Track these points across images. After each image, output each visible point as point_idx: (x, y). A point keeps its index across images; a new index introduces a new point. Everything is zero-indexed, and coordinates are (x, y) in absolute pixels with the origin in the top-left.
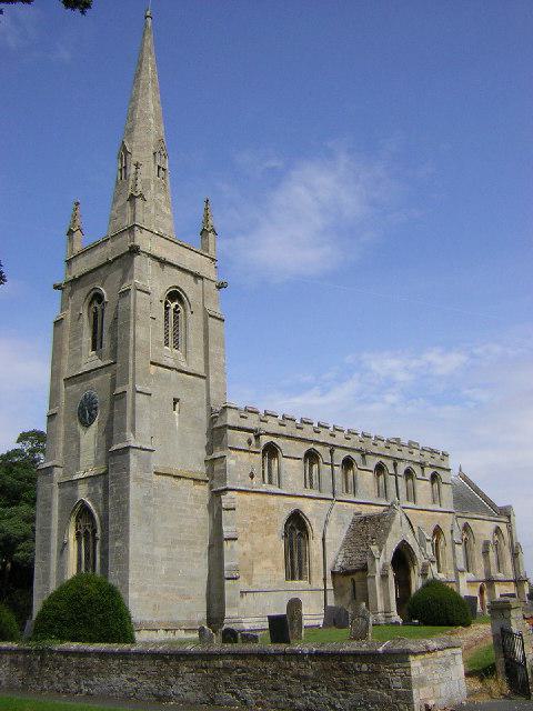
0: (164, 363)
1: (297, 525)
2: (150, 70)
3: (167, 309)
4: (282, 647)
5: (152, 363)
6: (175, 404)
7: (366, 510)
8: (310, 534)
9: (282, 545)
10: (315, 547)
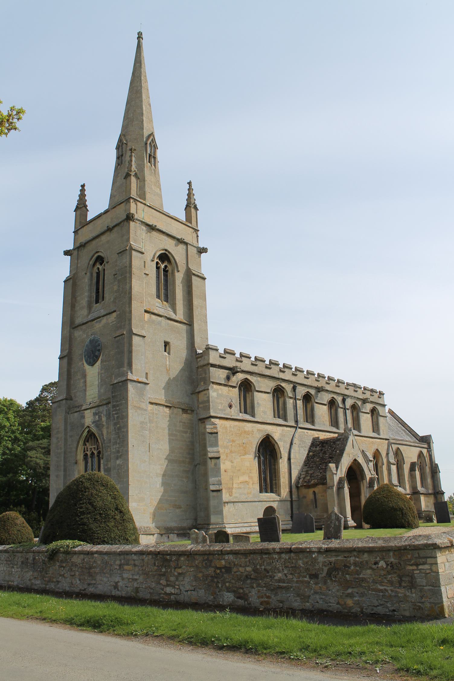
0: (156, 312)
1: (267, 450)
2: (362, 507)
3: (158, 268)
4: (273, 545)
5: (146, 311)
6: (165, 346)
7: (323, 436)
8: (279, 456)
9: (255, 464)
10: (283, 465)
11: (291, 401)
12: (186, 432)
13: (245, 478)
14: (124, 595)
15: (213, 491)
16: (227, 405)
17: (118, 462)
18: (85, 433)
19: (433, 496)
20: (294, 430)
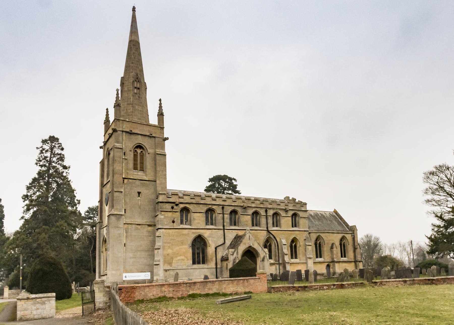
8: (208, 245)
9: (191, 250)
10: (210, 250)
12: (150, 236)
19: (353, 264)
20: (225, 231)
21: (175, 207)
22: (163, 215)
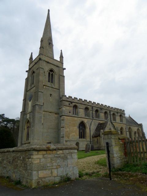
1: (82, 125)
6: (51, 95)
7: (101, 122)
8: (86, 127)
10: (88, 130)
11: (91, 112)
13: (74, 134)
14: (109, 170)
15: (62, 137)
16: (69, 112)
17: (33, 128)
18: (27, 121)
20: (92, 120)
21: (71, 104)
22: (64, 108)
